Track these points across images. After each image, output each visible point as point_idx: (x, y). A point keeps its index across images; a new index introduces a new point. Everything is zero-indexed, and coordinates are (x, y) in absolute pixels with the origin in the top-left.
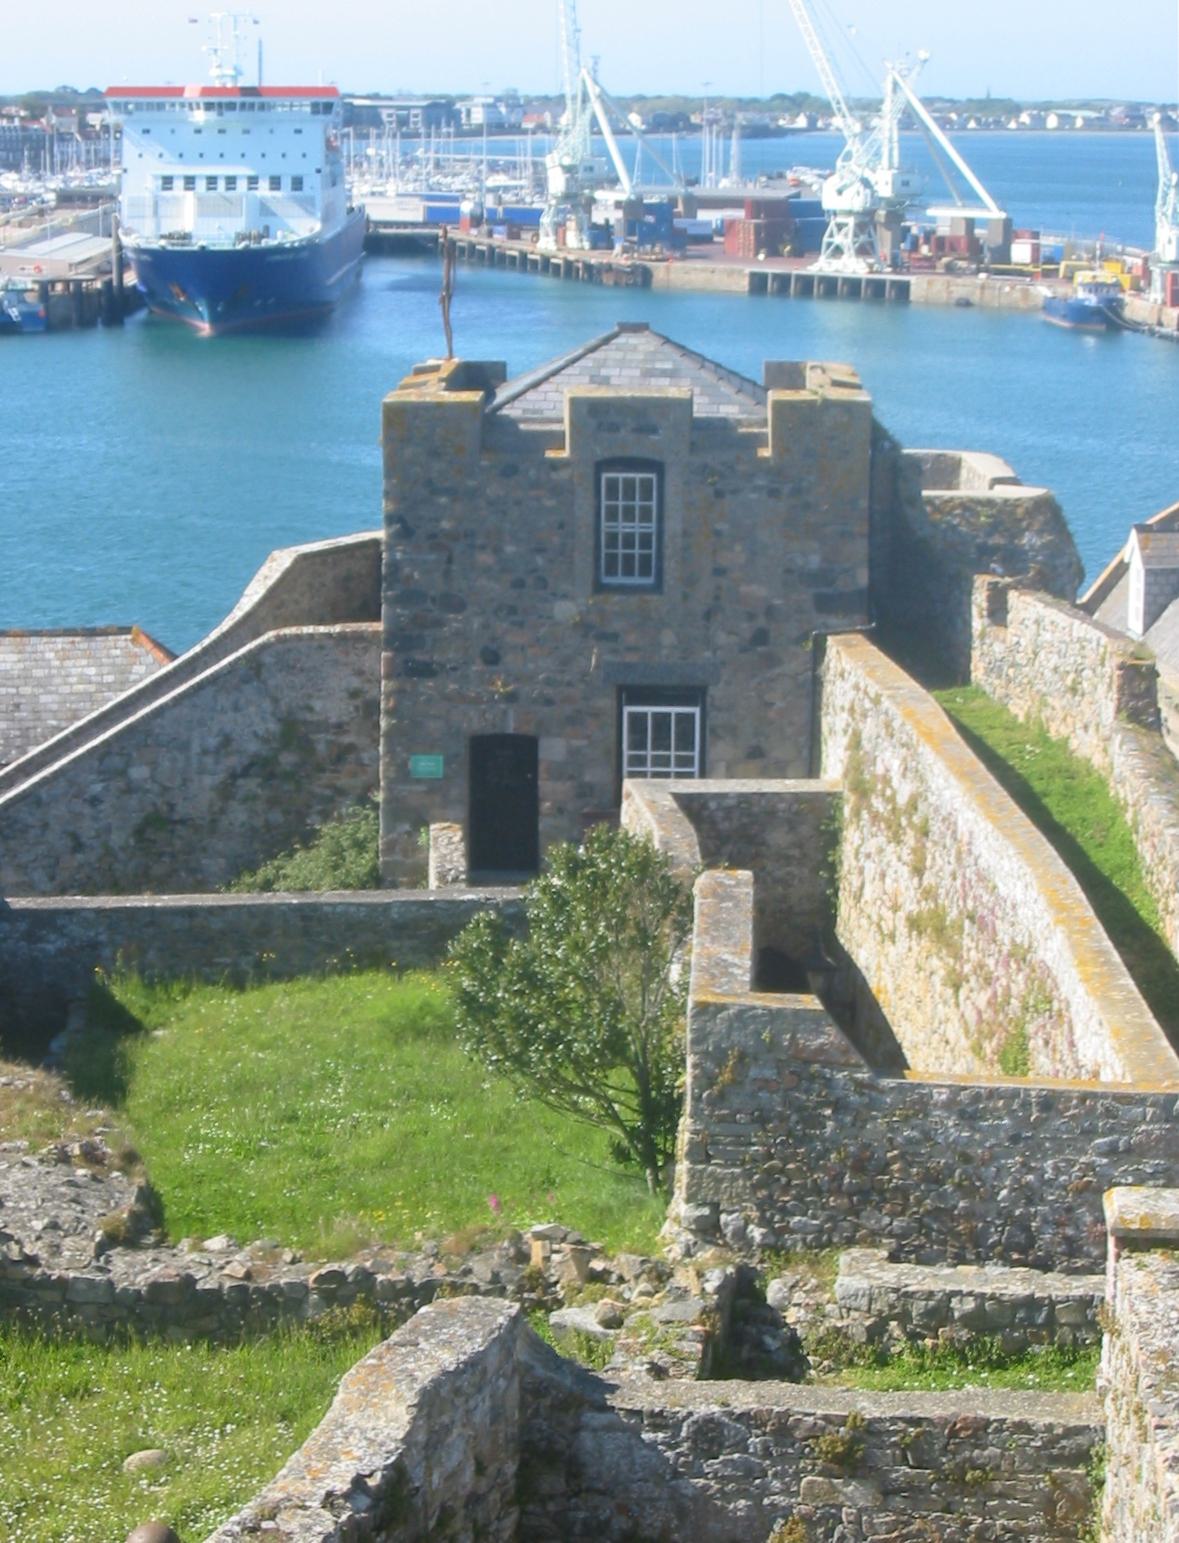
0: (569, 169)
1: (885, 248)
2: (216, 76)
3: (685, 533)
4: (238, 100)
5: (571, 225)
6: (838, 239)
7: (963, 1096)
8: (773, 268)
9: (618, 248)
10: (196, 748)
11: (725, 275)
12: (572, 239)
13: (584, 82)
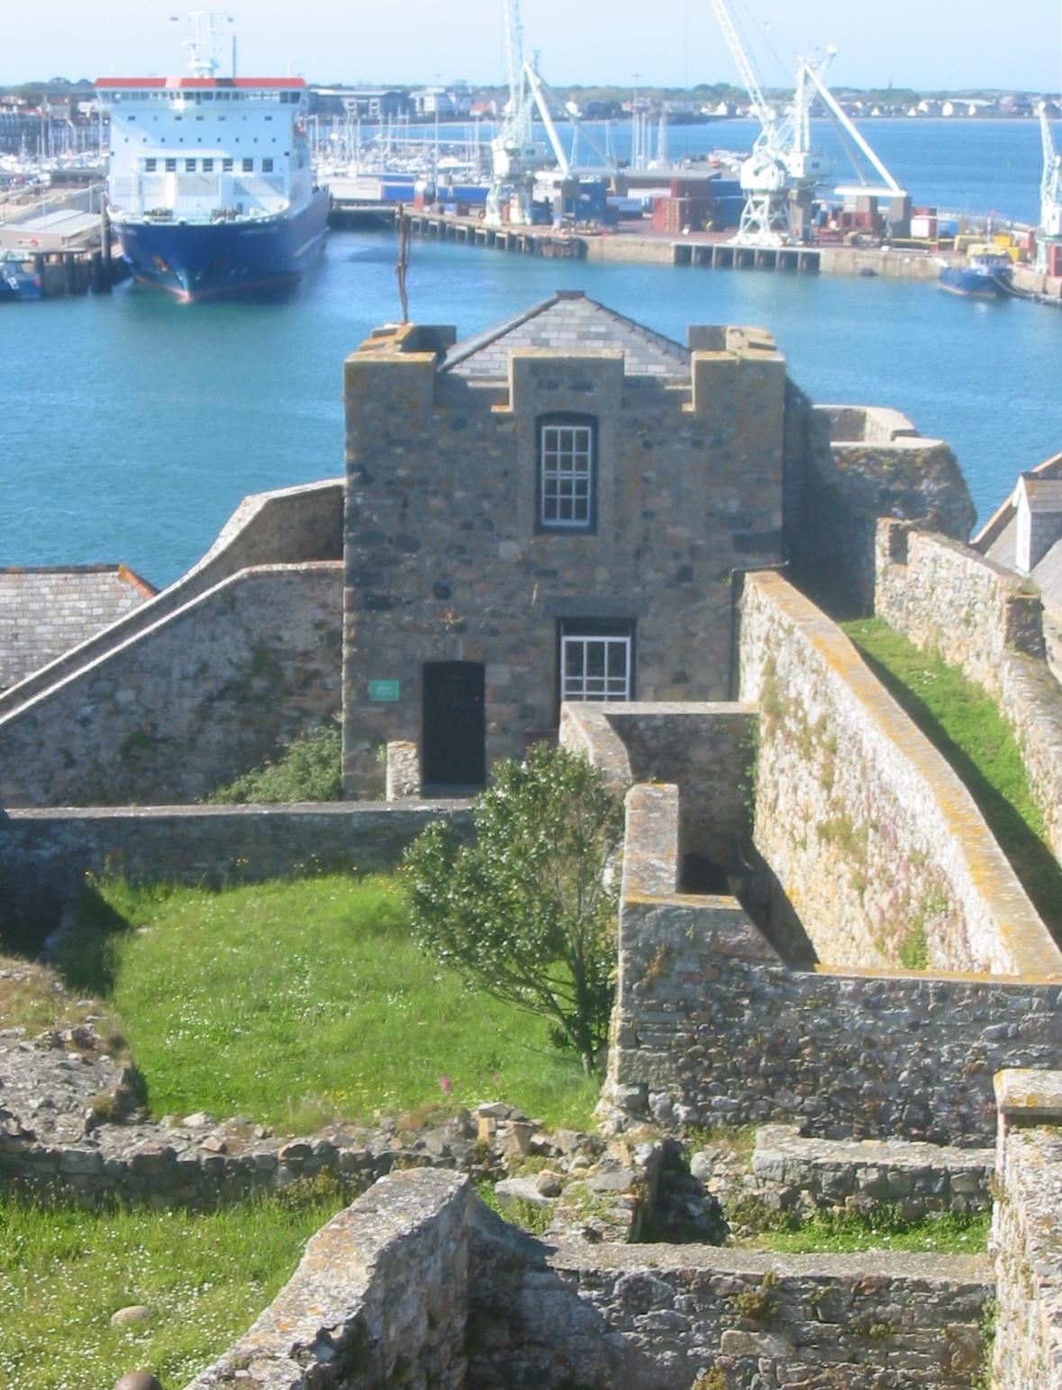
0: (512, 153)
1: (797, 223)
2: (195, 68)
3: (617, 481)
4: (215, 90)
5: (515, 203)
6: (755, 216)
7: (867, 987)
8: (696, 242)
9: (557, 223)
10: (176, 674)
11: (653, 247)
12: (516, 215)
13: (526, 74)
